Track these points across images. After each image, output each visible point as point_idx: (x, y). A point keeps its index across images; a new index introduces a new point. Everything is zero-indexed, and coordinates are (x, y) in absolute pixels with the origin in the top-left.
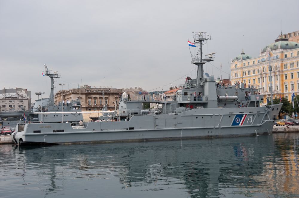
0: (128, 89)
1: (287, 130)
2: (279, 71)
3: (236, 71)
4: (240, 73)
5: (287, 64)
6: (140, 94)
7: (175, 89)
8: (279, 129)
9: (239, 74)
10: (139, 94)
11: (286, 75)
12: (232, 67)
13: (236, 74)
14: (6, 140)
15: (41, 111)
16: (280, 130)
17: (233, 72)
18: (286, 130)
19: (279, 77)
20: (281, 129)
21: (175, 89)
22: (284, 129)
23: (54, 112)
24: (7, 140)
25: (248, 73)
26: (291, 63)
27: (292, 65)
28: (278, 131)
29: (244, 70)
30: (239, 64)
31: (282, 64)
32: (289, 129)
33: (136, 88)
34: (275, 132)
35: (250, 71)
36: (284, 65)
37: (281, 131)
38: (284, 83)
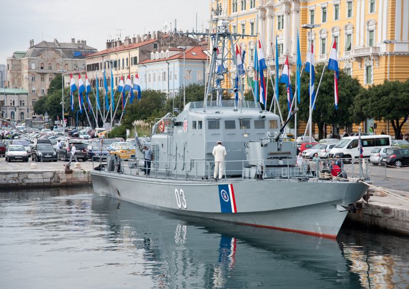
0: (45, 42)
1: (64, 179)
6: (78, 57)
7: (118, 44)
8: (30, 176)
10: (75, 57)
11: (312, 11)
14: (36, 193)
16: (34, 179)
18: (59, 178)
20: (40, 176)
21: (118, 44)
22: (50, 175)
23: (97, 102)
24: (34, 193)
25: (241, 3)
28: (27, 181)
32: (70, 176)
33: (73, 40)
34: (17, 184)
37: (41, 181)
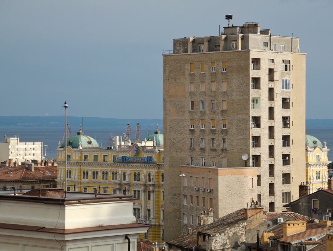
2: (154, 185)
3: (318, 169)
4: (77, 173)
5: (139, 173)
9: (75, 174)
12: (60, 158)
13: (69, 173)
15: (68, 149)
17: (62, 167)
19: (145, 195)
26: (103, 172)
27: (115, 175)
29: (85, 168)
30: (75, 155)
31: (158, 172)
35: (139, 173)
36: (82, 172)
38: (160, 206)
